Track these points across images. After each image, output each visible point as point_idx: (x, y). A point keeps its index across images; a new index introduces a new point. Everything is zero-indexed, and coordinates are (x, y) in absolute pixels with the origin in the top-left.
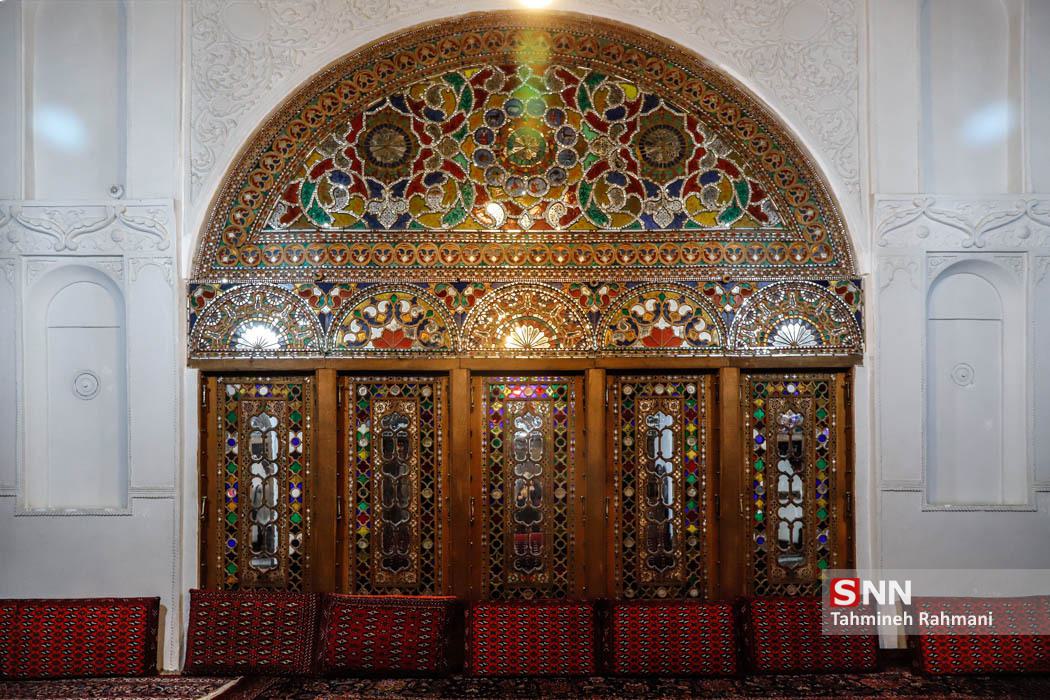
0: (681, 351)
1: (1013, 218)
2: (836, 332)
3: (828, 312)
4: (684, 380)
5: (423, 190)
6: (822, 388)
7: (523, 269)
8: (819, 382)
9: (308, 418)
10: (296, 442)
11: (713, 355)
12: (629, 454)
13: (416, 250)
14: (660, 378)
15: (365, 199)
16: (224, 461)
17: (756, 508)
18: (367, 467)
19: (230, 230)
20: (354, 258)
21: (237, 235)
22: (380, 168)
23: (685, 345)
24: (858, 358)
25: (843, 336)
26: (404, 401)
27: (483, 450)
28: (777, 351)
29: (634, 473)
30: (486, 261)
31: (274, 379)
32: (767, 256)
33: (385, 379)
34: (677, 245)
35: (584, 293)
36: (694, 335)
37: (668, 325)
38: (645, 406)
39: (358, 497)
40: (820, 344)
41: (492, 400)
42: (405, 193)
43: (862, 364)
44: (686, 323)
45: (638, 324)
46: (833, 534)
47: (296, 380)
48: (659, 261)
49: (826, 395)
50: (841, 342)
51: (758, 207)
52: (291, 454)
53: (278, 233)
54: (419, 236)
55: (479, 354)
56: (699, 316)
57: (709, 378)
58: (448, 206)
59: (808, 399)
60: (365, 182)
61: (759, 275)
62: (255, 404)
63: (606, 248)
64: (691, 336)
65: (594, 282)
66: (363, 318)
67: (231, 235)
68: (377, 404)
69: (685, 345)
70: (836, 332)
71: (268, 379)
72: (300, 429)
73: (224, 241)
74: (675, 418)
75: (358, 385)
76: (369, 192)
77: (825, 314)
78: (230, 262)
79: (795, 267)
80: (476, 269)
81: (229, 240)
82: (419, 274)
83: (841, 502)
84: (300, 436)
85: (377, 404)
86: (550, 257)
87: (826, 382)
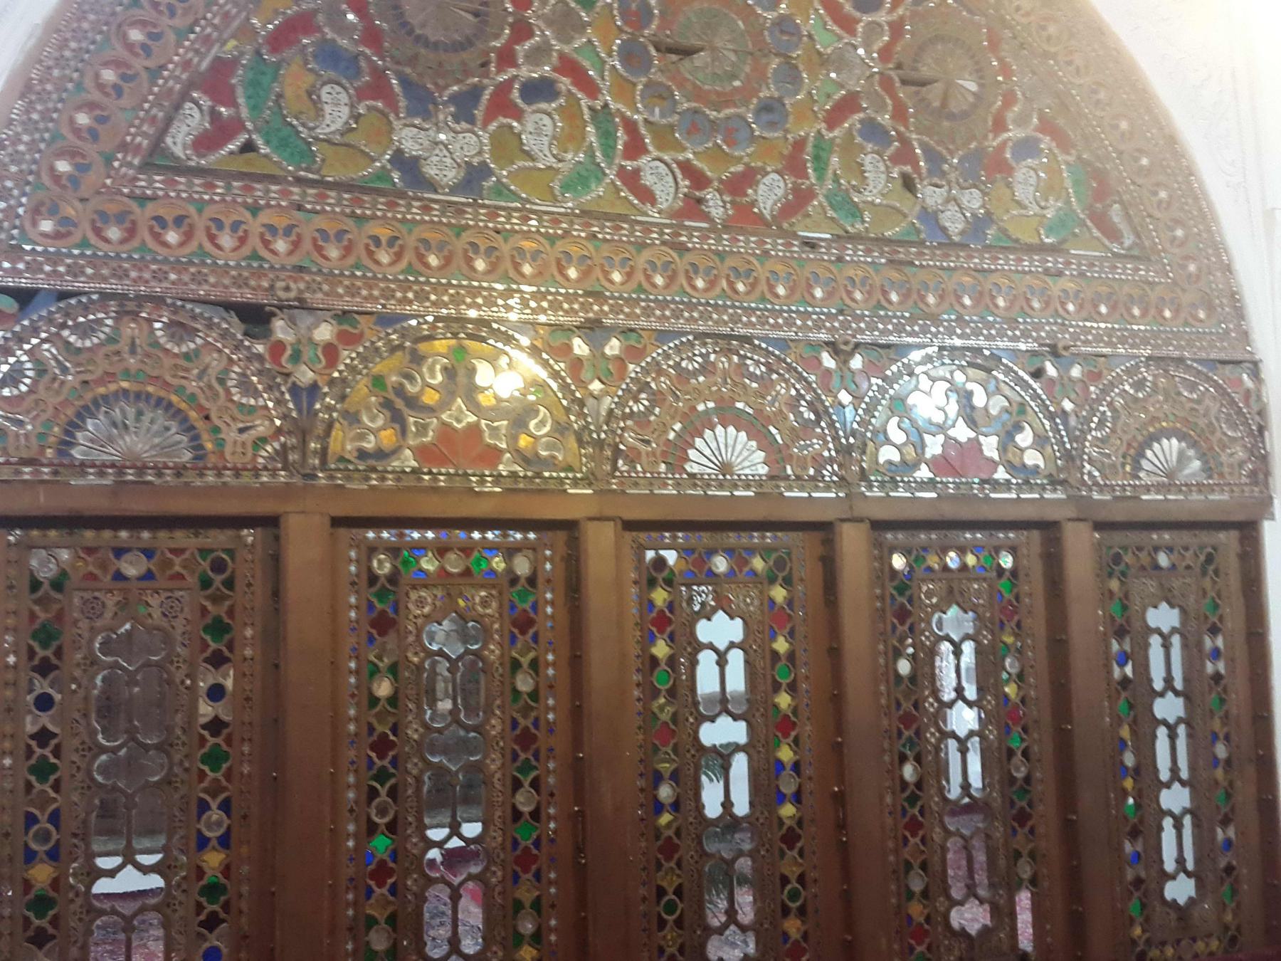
0: (996, 485)
1: (1009, 244)
2: (241, 431)
3: (222, 381)
4: (995, 542)
5: (518, 115)
6: (1210, 559)
7: (627, 301)
8: (233, 559)
9: (249, 632)
10: (216, 693)
11: (1096, 496)
12: (526, 710)
13: (506, 248)
14: (953, 535)
15: (392, 116)
16: (22, 752)
17: (1125, 794)
18: (392, 745)
19: (60, 155)
20: (370, 254)
21: (78, 167)
22: (423, 51)
23: (1001, 474)
24: (1265, 506)
25: (261, 441)
26: (472, 586)
27: (636, 693)
28: (1147, 489)
29: (918, 733)
30: (646, 285)
31: (162, 534)
32: (408, 257)
33: (430, 535)
34: (404, 229)
35: (577, 351)
36: (1014, 454)
37: (973, 435)
38: (421, 603)
39: (369, 820)
40: (1210, 477)
41: (652, 583)
42: (479, 113)
43: (1273, 514)
44: (406, 411)
45: (406, 411)
46: (1240, 833)
47: (218, 539)
48: (410, 264)
49: (1216, 572)
50: (255, 456)
51: (637, 172)
52: (204, 727)
53: (657, 225)
54: (509, 217)
55: (636, 485)
56: (1022, 417)
57: (561, 536)
58: (569, 156)
59: (179, 594)
60: (586, 110)
61: (1110, 344)
62: (111, 601)
63: (236, 217)
64: (1010, 456)
65: (846, 343)
66: (392, 396)
67: (63, 166)
68: (414, 595)
69: (1001, 474)
70: (241, 431)
71: (146, 535)
72: (227, 660)
73: (46, 179)
74: (979, 618)
75: (372, 550)
76: (403, 103)
77: (1214, 421)
78: (57, 236)
79: (385, 279)
80: (627, 301)
81: (56, 177)
82: (186, 278)
83: (1251, 770)
84: (1220, 642)
85: (414, 595)
86: (763, 287)
87: (230, 552)
